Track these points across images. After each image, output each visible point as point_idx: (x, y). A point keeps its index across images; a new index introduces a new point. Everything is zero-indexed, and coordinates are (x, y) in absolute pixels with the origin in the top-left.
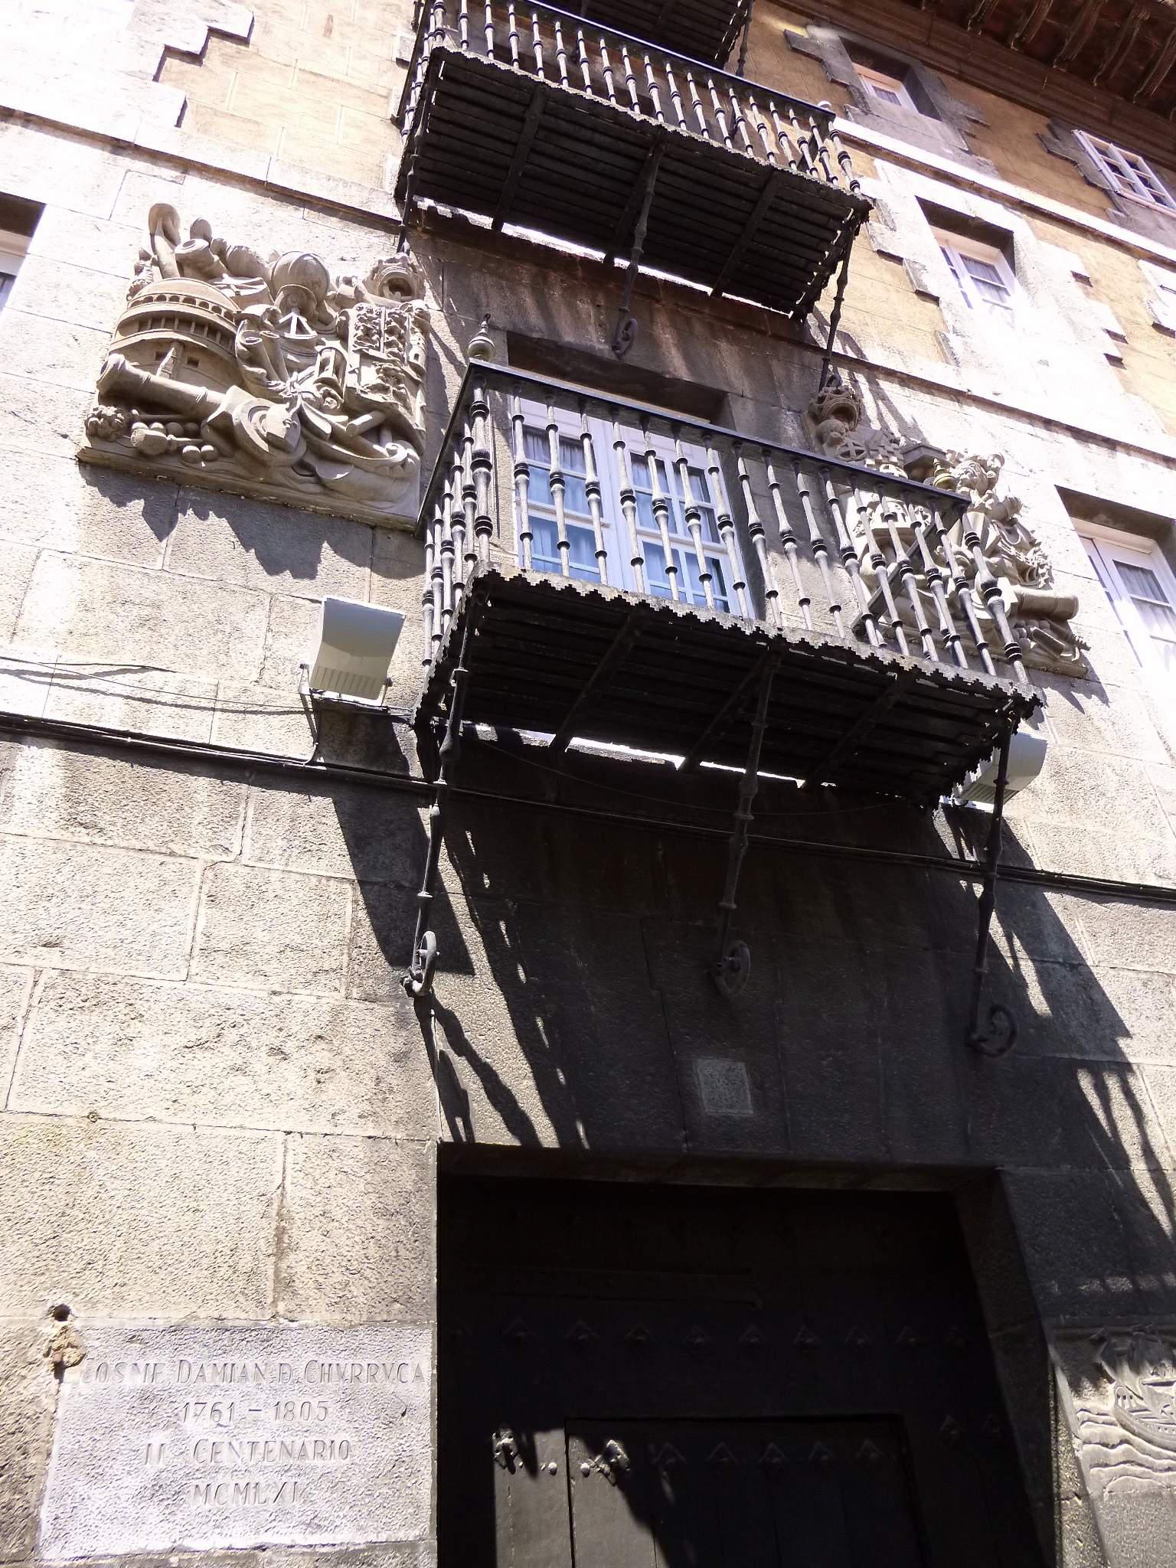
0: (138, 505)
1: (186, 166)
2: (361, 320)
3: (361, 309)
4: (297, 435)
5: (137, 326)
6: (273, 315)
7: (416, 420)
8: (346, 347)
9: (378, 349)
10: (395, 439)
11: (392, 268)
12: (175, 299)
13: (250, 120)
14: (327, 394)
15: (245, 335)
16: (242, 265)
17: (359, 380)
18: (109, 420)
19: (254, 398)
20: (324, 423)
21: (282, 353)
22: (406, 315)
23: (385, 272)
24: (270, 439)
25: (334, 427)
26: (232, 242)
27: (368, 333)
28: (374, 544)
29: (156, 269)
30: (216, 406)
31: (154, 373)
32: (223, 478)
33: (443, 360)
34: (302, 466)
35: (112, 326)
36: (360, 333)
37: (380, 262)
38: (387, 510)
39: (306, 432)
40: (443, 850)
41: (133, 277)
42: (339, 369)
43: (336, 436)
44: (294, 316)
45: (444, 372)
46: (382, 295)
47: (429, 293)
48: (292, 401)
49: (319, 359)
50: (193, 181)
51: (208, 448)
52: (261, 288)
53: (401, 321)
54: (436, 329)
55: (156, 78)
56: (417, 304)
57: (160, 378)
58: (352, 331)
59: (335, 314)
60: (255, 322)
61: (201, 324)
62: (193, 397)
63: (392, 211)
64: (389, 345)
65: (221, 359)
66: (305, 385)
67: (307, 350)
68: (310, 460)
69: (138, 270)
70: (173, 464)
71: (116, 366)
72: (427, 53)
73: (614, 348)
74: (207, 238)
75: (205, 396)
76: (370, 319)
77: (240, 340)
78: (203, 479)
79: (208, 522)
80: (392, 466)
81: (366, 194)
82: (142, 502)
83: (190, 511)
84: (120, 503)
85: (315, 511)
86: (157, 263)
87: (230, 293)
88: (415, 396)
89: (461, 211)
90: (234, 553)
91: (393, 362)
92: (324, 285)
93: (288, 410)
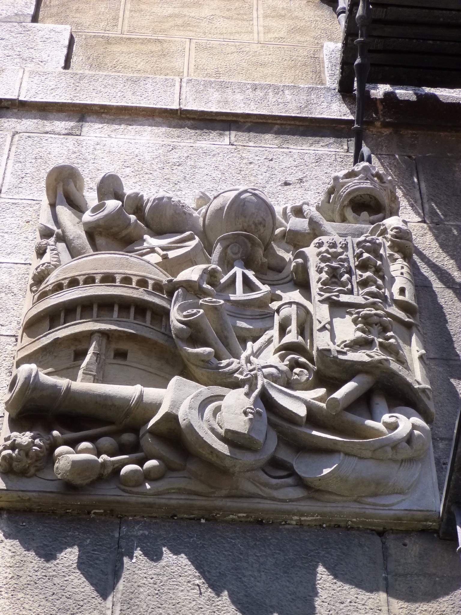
0: (70, 556)
1: (81, 113)
2: (324, 259)
3: (320, 245)
4: (263, 426)
5: (47, 323)
6: (211, 276)
7: (417, 376)
8: (308, 297)
9: (351, 292)
10: (391, 408)
11: (354, 184)
12: (90, 280)
13: (149, 41)
14: (295, 364)
15: (182, 309)
16: (165, 220)
17: (333, 337)
18: (25, 450)
19: (203, 388)
20: (295, 402)
21: (229, 320)
22: (380, 240)
23: (344, 191)
24: (231, 438)
25: (310, 407)
26: (150, 194)
27: (334, 276)
28: (386, 556)
29: (61, 246)
30: (157, 406)
31: (75, 380)
32: (175, 500)
33: (437, 285)
34: (275, 464)
35: (15, 326)
36: (324, 276)
37: (336, 179)
38: (398, 506)
39: (274, 419)
41: (36, 262)
42: (305, 327)
43: (314, 418)
44: (238, 271)
45: (441, 301)
46: (344, 220)
47: (404, 203)
48: (251, 382)
49: (277, 319)
50: (94, 132)
51: (152, 463)
52: (192, 244)
53: (374, 249)
54: (420, 247)
55: (35, 19)
56: (391, 222)
57: (82, 384)
58: (314, 276)
59: (288, 256)
60: (192, 289)
61: (125, 305)
62: (125, 401)
63: (338, 110)
64: (364, 284)
65: (155, 343)
66: (264, 356)
67: (260, 311)
68: (285, 455)
69: (41, 252)
70: (110, 493)
71: (28, 378)
74: (118, 196)
75: (141, 396)
76: (335, 256)
77: (176, 316)
78: (150, 505)
79: (163, 563)
80: (395, 445)
81: (303, 97)
82: (75, 550)
83: (138, 552)
84: (48, 555)
85: (300, 524)
86: (62, 238)
87: (154, 258)
88: (410, 344)
89: (428, 90)
90: (202, 600)
91: (373, 305)
92: (269, 219)
93: (248, 395)
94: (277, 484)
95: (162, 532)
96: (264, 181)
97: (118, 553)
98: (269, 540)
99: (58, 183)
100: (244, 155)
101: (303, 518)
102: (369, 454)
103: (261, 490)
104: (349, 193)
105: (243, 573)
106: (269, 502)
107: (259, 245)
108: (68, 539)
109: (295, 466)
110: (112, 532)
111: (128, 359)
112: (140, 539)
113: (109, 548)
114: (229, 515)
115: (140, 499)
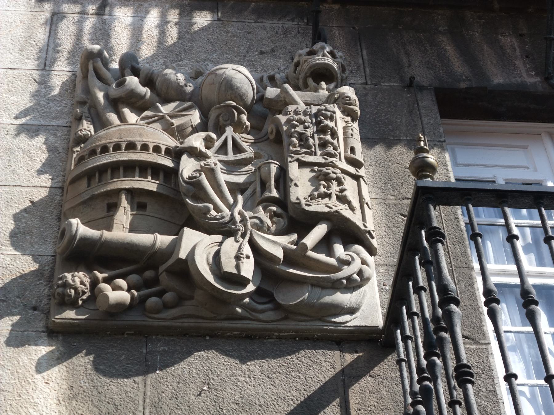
25: (286, 251)
40: (333, 320)
72: (324, 170)
73: (547, 79)
94: (262, 310)
95: (178, 348)
96: (245, 51)
97: (146, 366)
98: (257, 351)
99: (89, 61)
100: (229, 29)
101: (281, 334)
102: (330, 285)
103: (250, 314)
104: (310, 67)
105: (238, 379)
106: (255, 323)
107: (244, 113)
108: (108, 355)
109: (275, 295)
110: (141, 349)
111: (147, 210)
112: (161, 354)
113: (139, 362)
114: (227, 333)
115: (161, 323)
